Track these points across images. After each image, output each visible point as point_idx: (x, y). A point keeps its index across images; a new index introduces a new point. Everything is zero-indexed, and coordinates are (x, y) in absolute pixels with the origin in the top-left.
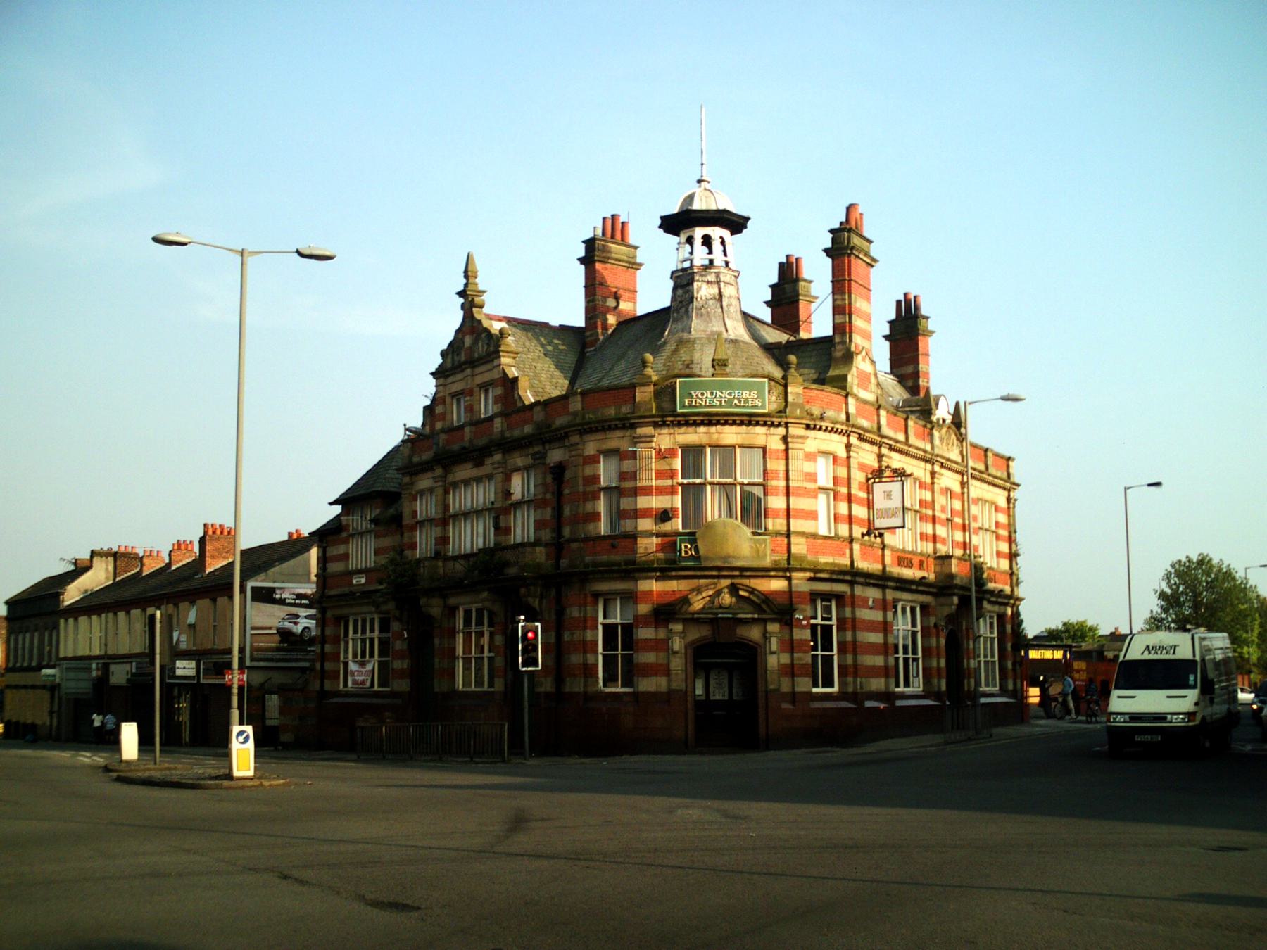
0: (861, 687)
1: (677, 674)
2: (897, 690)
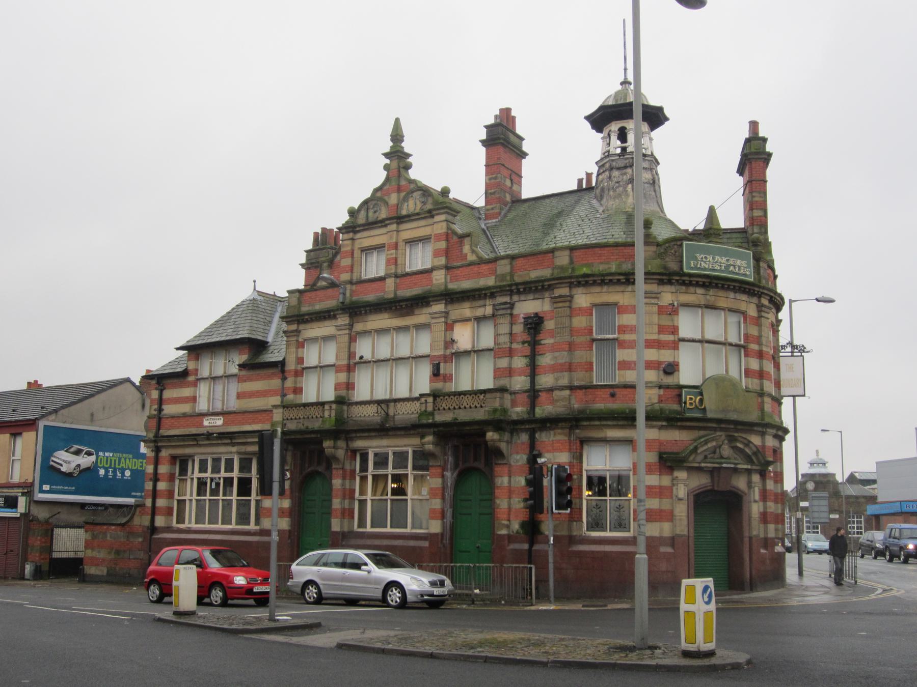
1: (680, 520)
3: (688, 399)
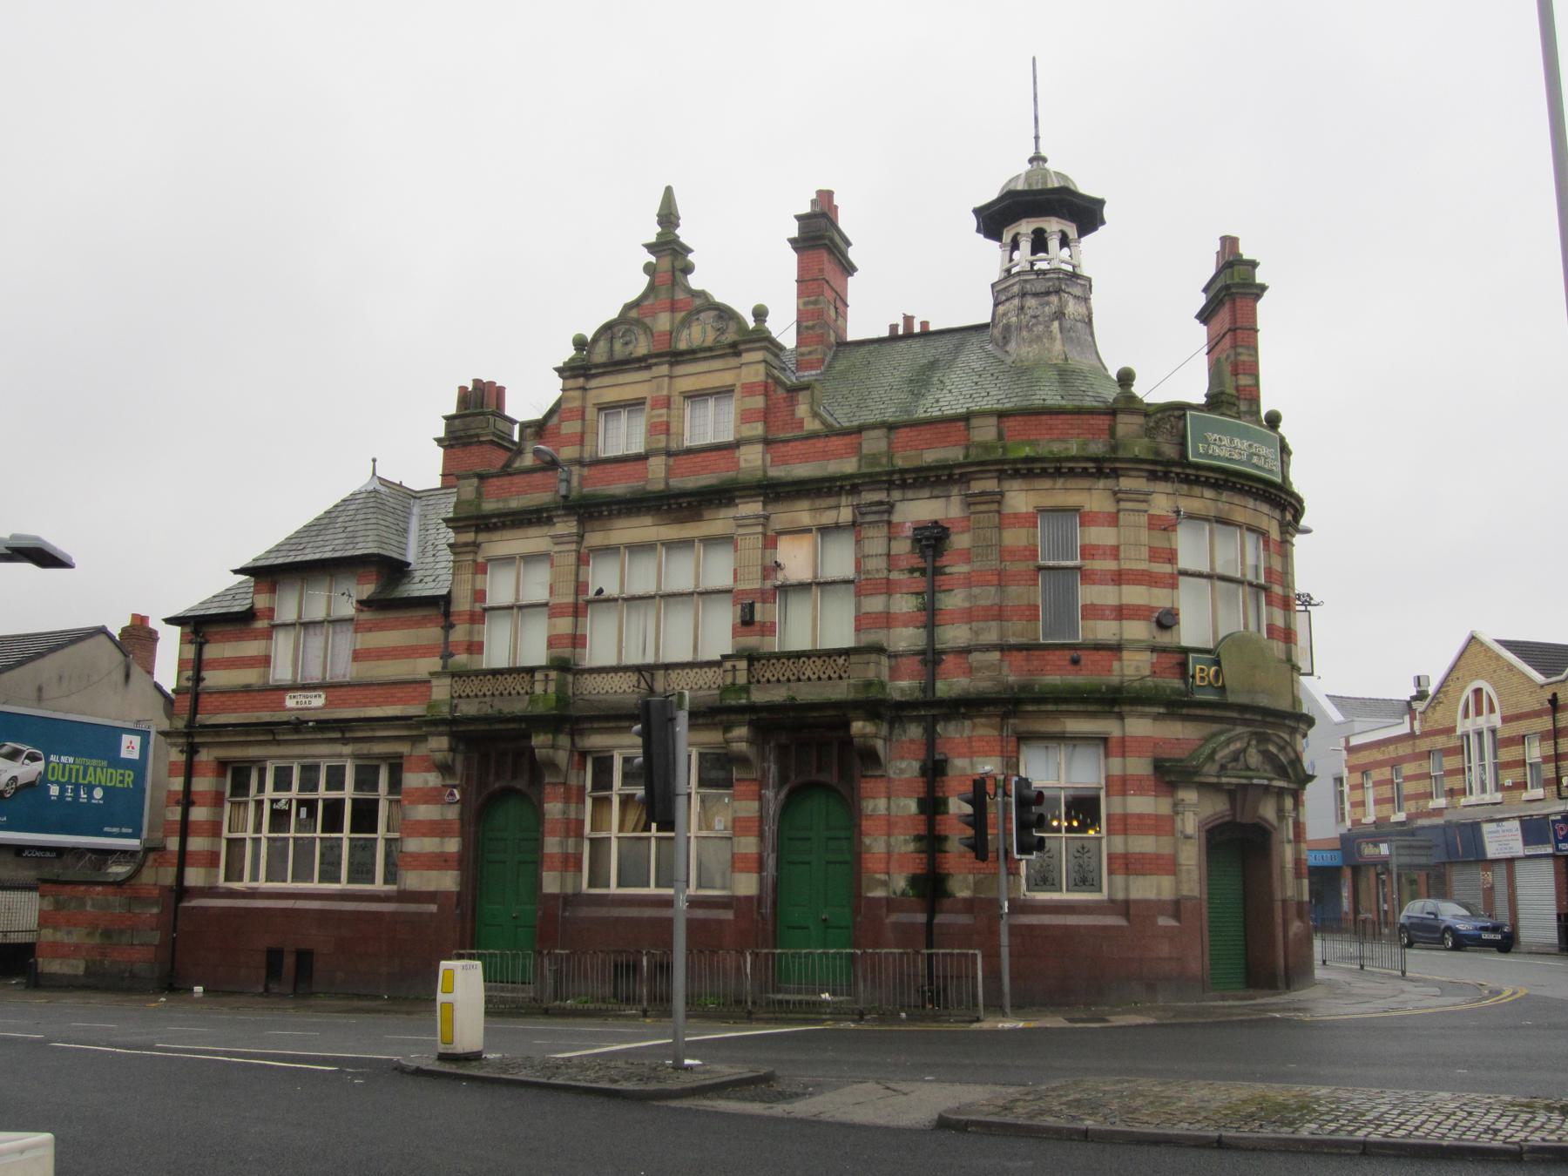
1: (1189, 872)
3: (1198, 670)
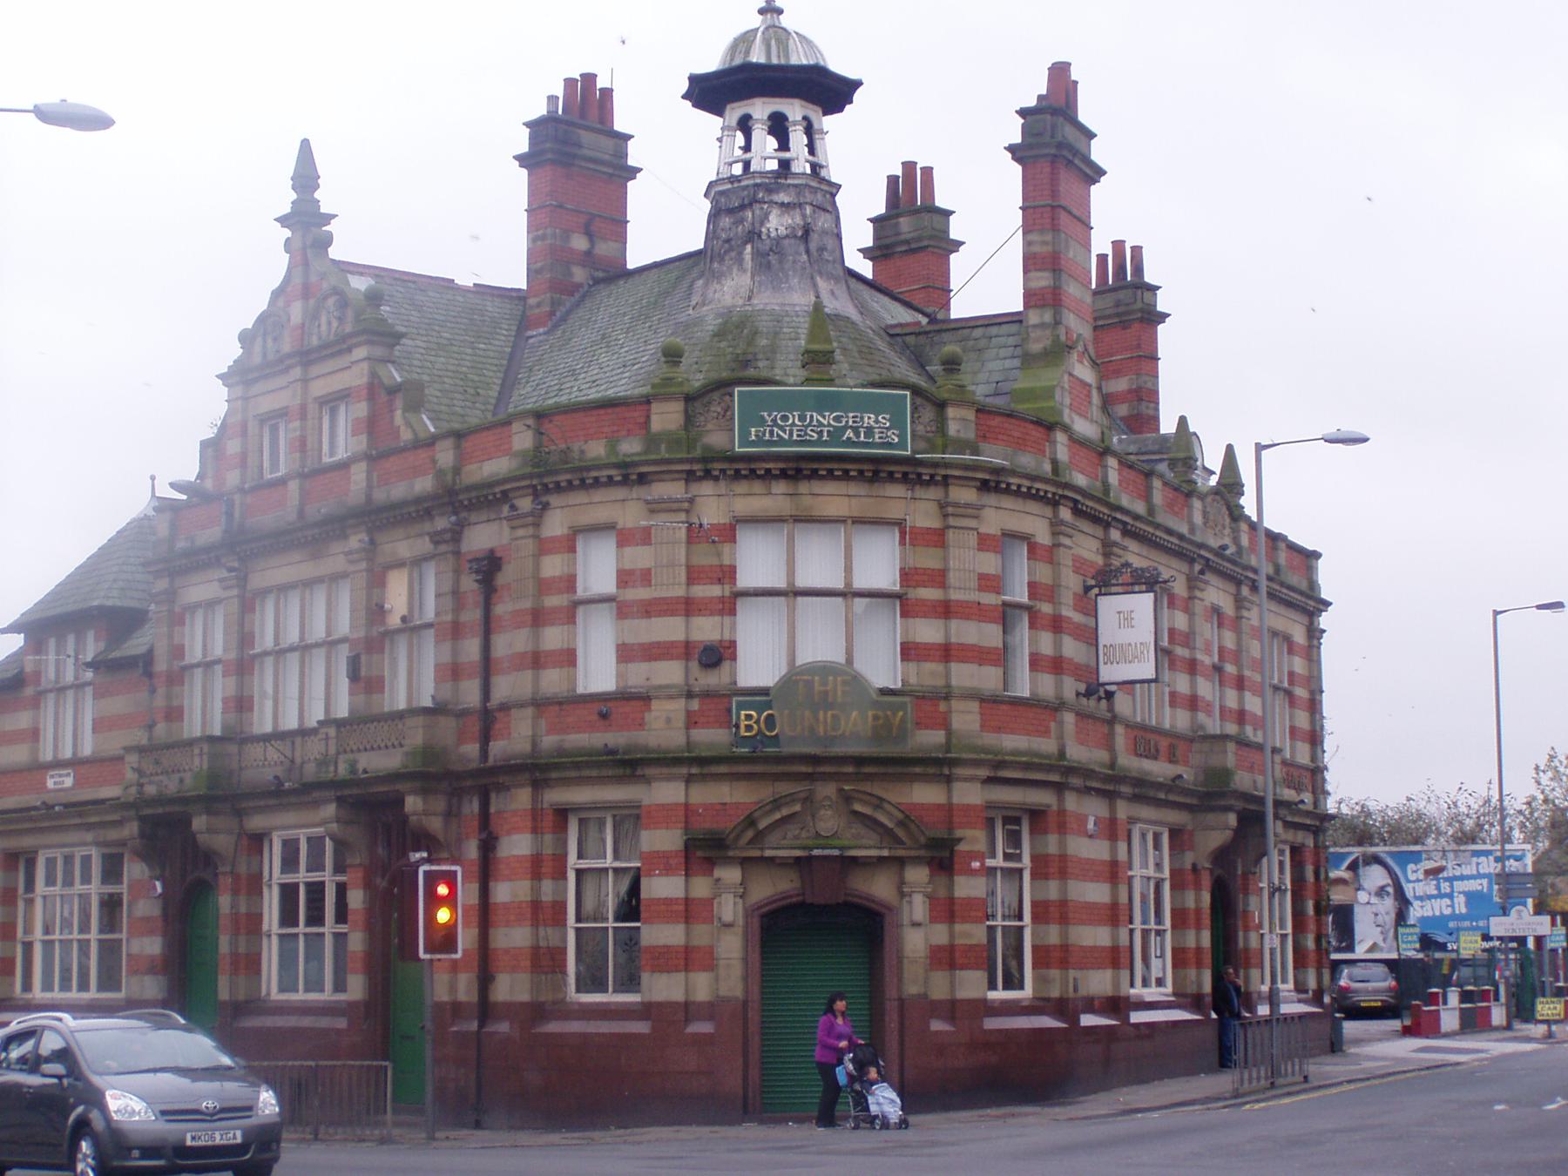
0: (1076, 990)
2: (1132, 991)
3: (743, 717)
